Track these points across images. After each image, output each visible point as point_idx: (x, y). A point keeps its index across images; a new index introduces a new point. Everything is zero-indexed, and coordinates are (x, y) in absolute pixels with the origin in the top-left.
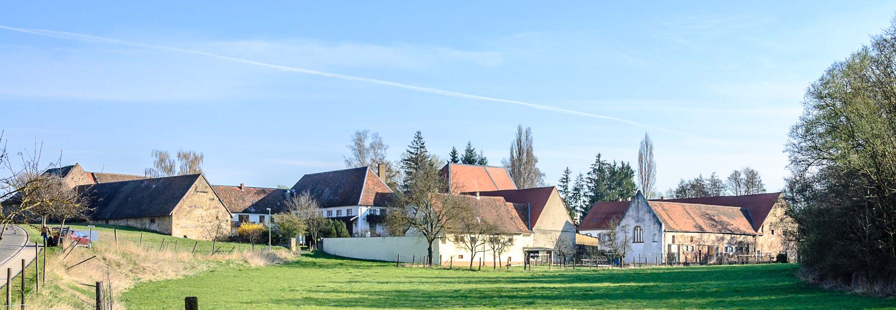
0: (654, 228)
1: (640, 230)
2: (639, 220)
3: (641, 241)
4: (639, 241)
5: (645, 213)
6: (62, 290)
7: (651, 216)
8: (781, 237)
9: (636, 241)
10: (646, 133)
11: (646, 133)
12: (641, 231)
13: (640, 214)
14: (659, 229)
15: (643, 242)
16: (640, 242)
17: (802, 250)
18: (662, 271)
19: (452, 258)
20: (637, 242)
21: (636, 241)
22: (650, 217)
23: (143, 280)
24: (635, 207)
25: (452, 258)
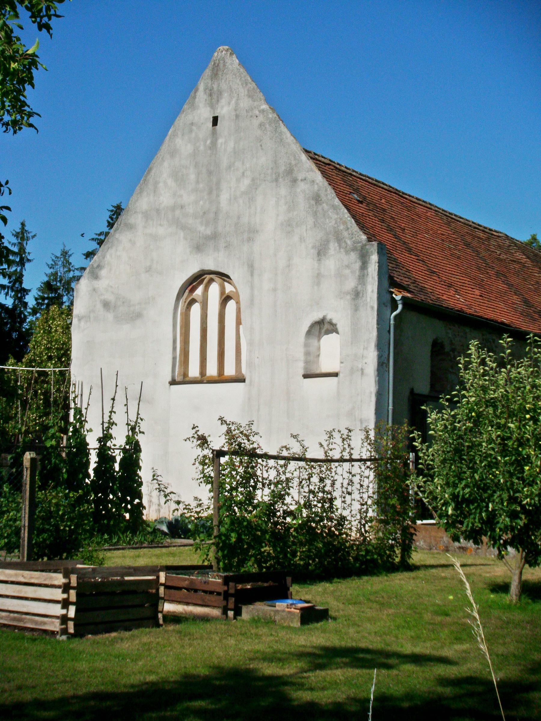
0: (318, 278)
1: (225, 299)
2: (214, 237)
3: (230, 370)
4: (212, 370)
5: (254, 185)
6: (281, 140)
7: (302, 204)
8: (349, 445)
9: (194, 371)
10: (63, 16)
11: (63, 16)
12: (231, 305)
13: (224, 197)
14: (351, 284)
15: (242, 380)
16: (221, 379)
17: (478, 641)
18: (22, 535)
19: (126, 389)
20: (203, 379)
21: (194, 371)
22: (292, 206)
23: (108, 564)
24: (195, 154)
25: (126, 389)
